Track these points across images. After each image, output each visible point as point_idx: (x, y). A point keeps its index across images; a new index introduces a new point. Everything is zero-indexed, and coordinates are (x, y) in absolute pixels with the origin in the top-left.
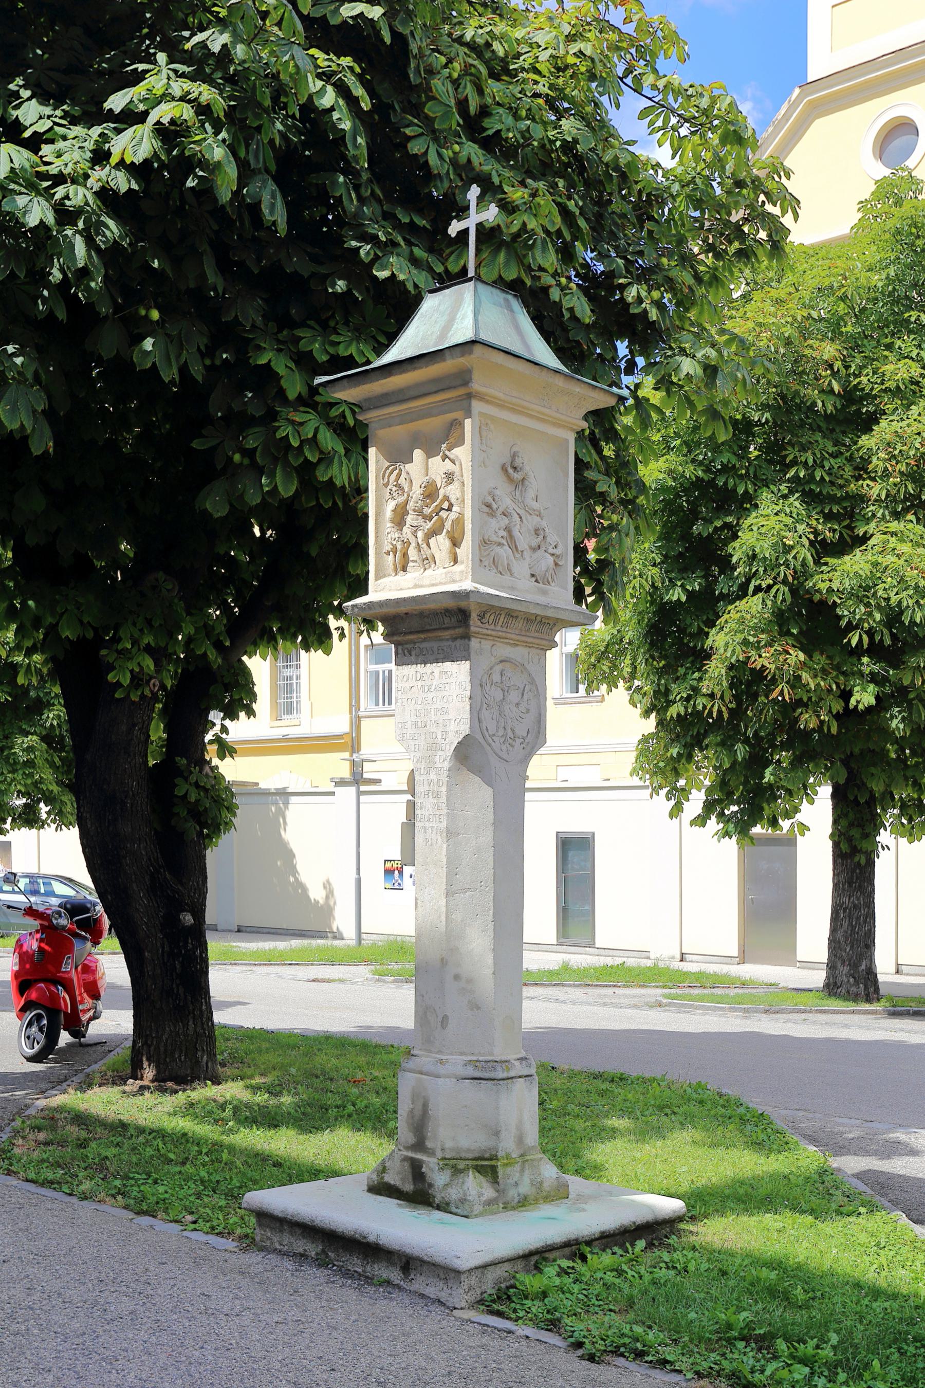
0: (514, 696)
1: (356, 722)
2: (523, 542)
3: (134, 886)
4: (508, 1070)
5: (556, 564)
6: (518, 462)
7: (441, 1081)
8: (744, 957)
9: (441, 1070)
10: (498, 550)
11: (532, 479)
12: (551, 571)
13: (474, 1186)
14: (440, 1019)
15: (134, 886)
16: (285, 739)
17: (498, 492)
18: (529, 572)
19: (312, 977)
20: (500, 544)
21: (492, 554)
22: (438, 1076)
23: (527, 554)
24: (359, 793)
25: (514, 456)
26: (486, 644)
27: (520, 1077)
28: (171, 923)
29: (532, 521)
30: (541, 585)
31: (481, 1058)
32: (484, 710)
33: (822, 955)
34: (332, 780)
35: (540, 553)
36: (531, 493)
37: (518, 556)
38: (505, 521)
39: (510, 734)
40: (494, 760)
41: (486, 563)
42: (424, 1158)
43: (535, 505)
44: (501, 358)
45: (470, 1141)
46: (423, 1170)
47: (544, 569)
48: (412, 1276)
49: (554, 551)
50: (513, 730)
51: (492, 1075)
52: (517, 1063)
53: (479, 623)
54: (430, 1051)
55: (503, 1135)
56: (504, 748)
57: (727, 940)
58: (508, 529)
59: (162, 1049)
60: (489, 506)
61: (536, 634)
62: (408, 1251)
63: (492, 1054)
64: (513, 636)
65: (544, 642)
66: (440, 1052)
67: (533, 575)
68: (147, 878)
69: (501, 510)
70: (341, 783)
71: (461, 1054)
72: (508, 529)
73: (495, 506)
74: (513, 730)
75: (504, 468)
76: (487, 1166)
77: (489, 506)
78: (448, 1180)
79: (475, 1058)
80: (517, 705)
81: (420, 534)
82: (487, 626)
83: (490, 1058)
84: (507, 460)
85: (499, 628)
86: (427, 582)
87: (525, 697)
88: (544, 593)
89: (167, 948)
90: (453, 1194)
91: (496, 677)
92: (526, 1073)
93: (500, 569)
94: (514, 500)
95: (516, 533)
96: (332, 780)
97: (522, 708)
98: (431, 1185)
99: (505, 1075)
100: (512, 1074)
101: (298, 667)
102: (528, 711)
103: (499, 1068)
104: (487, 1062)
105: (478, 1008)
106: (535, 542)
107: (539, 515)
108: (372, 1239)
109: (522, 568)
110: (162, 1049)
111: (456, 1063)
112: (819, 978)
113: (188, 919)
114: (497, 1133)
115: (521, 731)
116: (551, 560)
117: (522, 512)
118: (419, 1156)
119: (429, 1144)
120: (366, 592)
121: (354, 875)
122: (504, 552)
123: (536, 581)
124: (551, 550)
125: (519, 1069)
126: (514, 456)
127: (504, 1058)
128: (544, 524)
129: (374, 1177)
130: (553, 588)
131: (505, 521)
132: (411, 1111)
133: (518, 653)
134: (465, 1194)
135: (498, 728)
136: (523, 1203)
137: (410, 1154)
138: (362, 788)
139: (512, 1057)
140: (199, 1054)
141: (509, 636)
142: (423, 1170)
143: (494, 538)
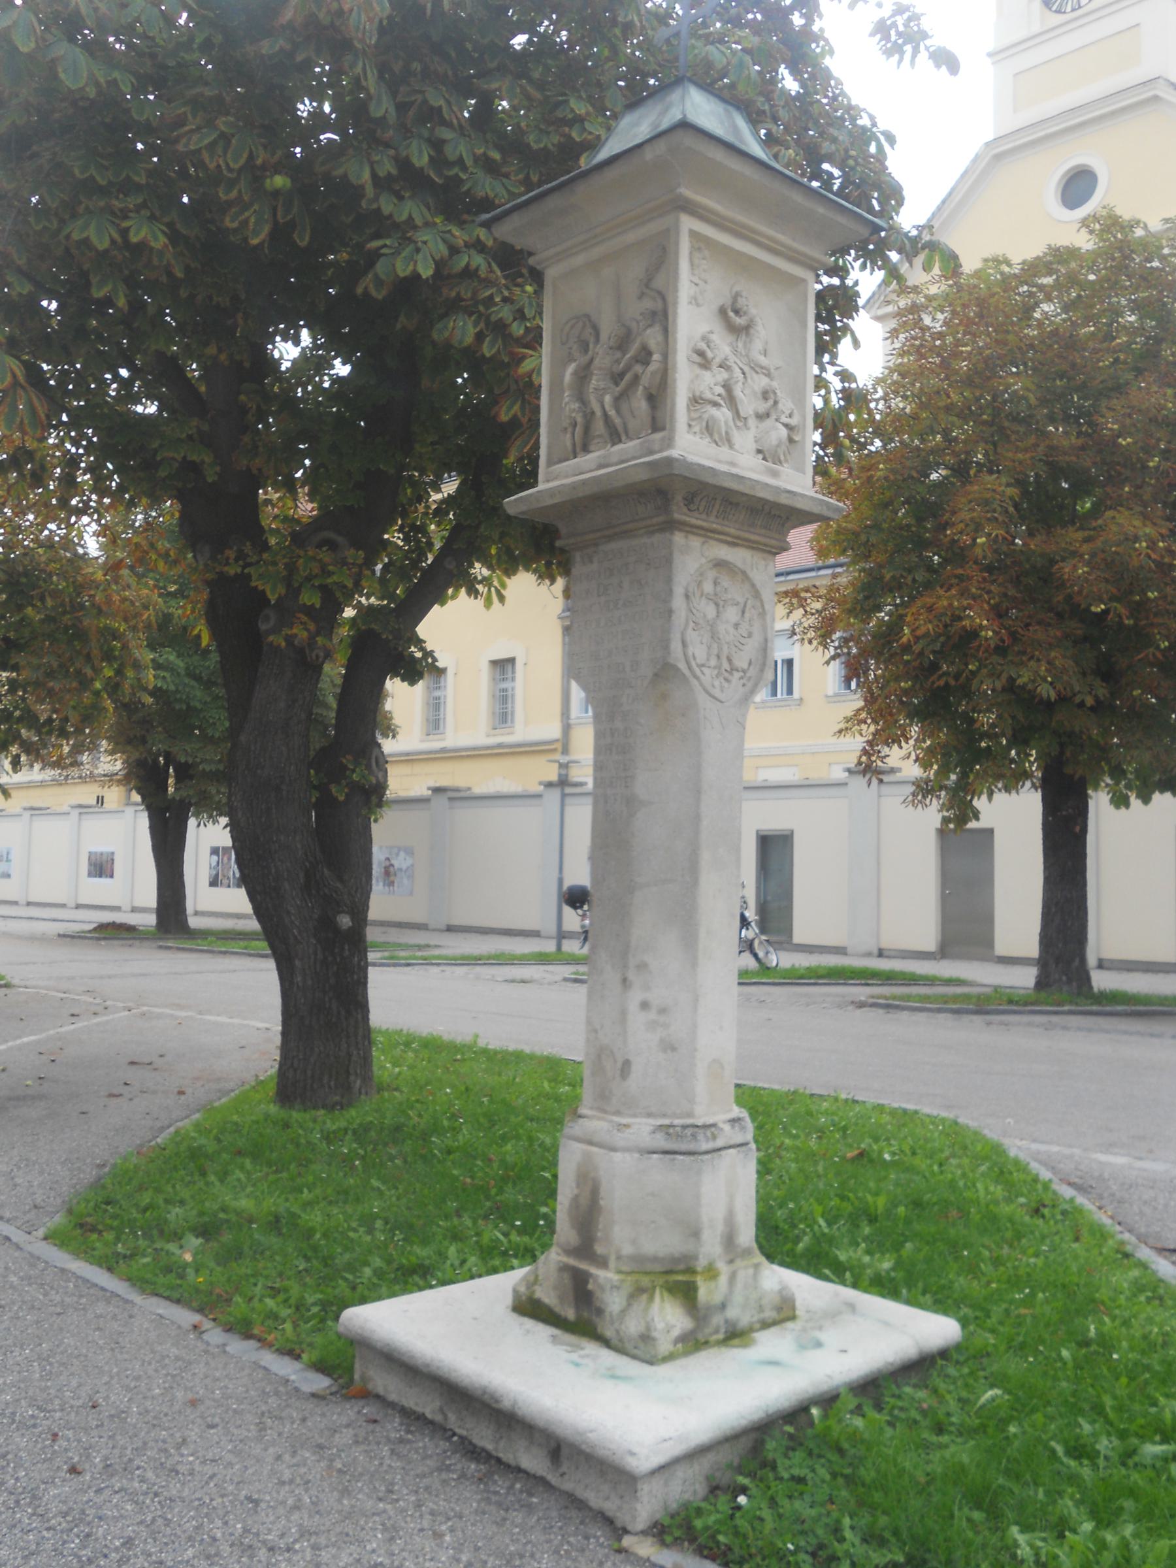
0: (732, 614)
1: (567, 728)
2: (749, 405)
3: (286, 885)
4: (714, 1137)
5: (791, 440)
6: (741, 302)
7: (617, 1156)
8: (944, 951)
9: (619, 1139)
10: (713, 411)
11: (760, 328)
12: (783, 447)
13: (668, 1317)
14: (619, 1065)
15: (286, 885)
16: (500, 746)
17: (714, 337)
18: (754, 447)
19: (509, 977)
20: (716, 404)
21: (706, 416)
22: (613, 1149)
23: (752, 422)
24: (564, 796)
25: (736, 297)
26: (695, 542)
27: (730, 1147)
28: (327, 924)
29: (762, 382)
30: (770, 464)
31: (677, 1122)
32: (690, 631)
33: (1032, 949)
34: (540, 783)
35: (769, 422)
36: (758, 345)
37: (739, 424)
38: (723, 375)
39: (726, 665)
40: (702, 698)
41: (697, 429)
42: (593, 1270)
43: (762, 360)
44: (719, 155)
45: (663, 1243)
46: (590, 1287)
47: (774, 443)
48: (564, 1469)
49: (787, 421)
50: (729, 660)
51: (692, 1147)
52: (727, 1127)
53: (685, 510)
54: (605, 1112)
55: (706, 1235)
56: (717, 683)
57: (927, 937)
58: (727, 387)
59: (309, 1073)
60: (701, 354)
61: (763, 531)
62: (560, 1431)
63: (690, 1115)
64: (732, 531)
65: (773, 542)
66: (618, 1113)
67: (759, 451)
68: (302, 875)
69: (717, 360)
70: (549, 785)
71: (650, 1115)
72: (727, 387)
73: (709, 354)
74: (729, 660)
75: (722, 311)
76: (680, 1280)
77: (701, 354)
78: (624, 1303)
79: (667, 1122)
80: (736, 626)
81: (608, 399)
82: (696, 514)
83: (689, 1121)
84: (728, 302)
85: (712, 518)
86: (614, 459)
87: (747, 615)
88: (775, 474)
89: (320, 956)
90: (632, 1327)
91: (708, 587)
92: (739, 1139)
93: (716, 437)
94: (735, 352)
95: (738, 392)
96: (540, 783)
97: (743, 630)
98: (600, 1312)
99: (710, 1145)
100: (720, 1143)
101: (513, 679)
102: (750, 635)
103: (701, 1137)
104: (684, 1127)
105: (674, 1049)
106: (762, 407)
107: (768, 375)
108: (506, 1404)
109: (745, 440)
110: (309, 1073)
111: (642, 1130)
112: (1026, 978)
113: (345, 921)
114: (696, 1234)
115: (741, 662)
116: (784, 432)
117: (746, 369)
118: (583, 1266)
119: (599, 1249)
120: (535, 484)
121: (556, 874)
122: (723, 414)
123: (764, 459)
124: (784, 419)
125: (729, 1135)
126: (736, 297)
127: (710, 1120)
128: (775, 384)
129: (523, 1289)
130: (786, 470)
131: (723, 375)
132: (575, 1199)
133: (738, 556)
134: (648, 1328)
135: (709, 655)
136: (735, 1336)
137: (572, 1262)
138: (568, 790)
139: (720, 1118)
140: (352, 1078)
141: (727, 530)
142: (590, 1287)
143: (708, 395)
